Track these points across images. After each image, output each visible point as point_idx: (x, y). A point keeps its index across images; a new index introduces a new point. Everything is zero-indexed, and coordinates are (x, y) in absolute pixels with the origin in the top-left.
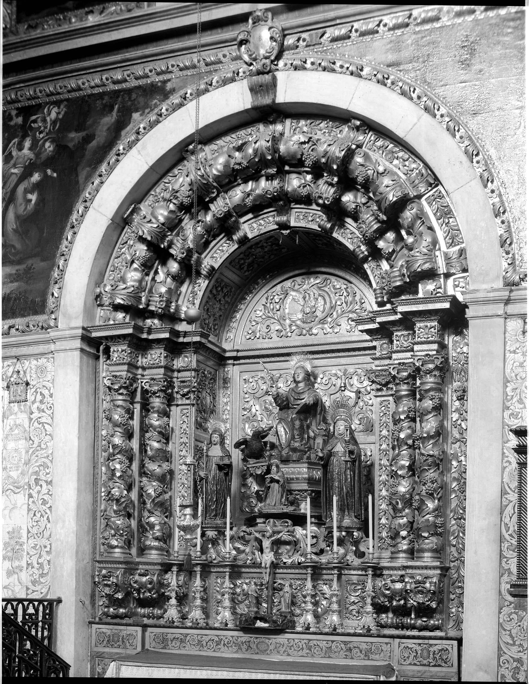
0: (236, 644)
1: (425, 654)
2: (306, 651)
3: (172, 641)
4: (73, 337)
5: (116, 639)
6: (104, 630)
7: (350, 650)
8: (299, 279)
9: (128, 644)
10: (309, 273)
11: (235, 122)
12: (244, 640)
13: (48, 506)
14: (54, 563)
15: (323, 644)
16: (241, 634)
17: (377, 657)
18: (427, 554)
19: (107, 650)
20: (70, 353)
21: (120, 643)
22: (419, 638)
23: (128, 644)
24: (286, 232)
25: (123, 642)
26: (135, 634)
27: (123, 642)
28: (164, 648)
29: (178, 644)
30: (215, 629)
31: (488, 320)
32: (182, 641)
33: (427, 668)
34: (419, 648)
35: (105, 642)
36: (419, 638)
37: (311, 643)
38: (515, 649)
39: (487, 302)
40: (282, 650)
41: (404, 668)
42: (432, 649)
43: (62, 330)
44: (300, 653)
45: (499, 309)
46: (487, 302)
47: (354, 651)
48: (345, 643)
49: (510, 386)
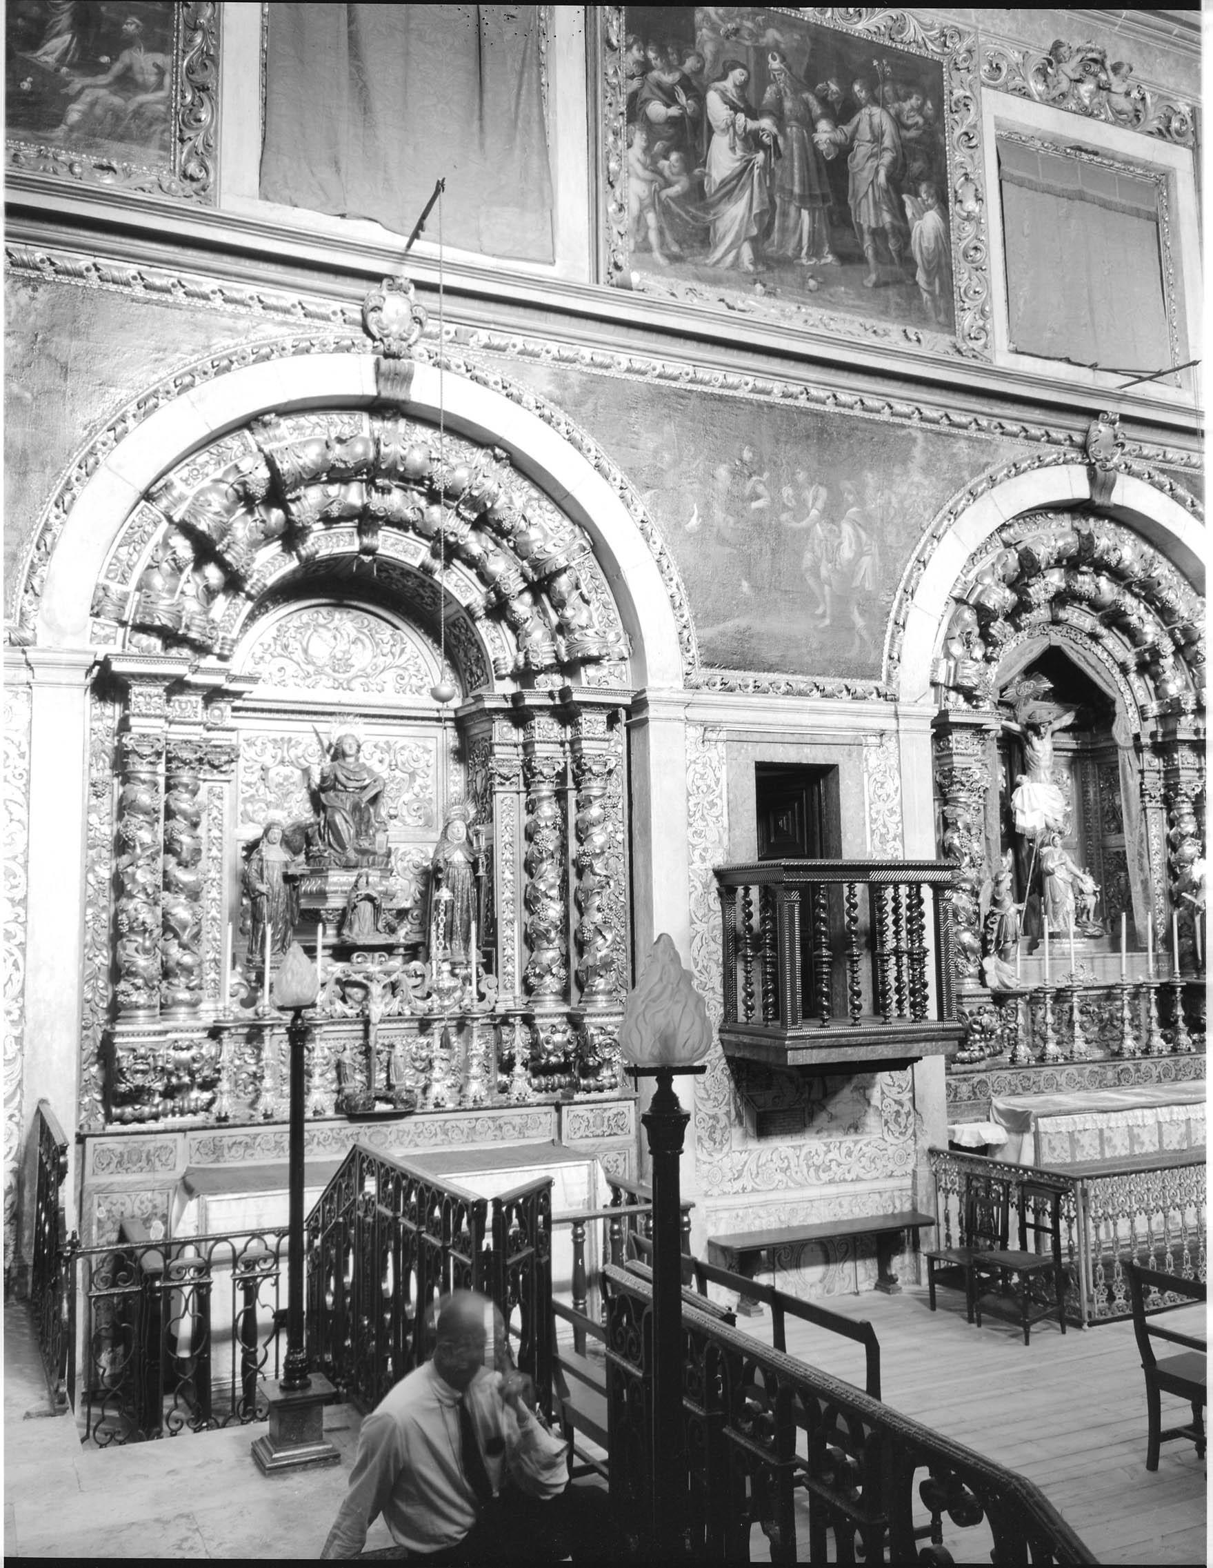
0: (336, 1140)
1: (598, 1122)
2: (441, 1137)
3: (230, 1148)
4: (74, 665)
5: (135, 1158)
6: (111, 1146)
7: (500, 1127)
8: (324, 610)
9: (158, 1164)
10: (339, 605)
11: (353, 402)
12: (349, 1132)
13: (17, 941)
14: (31, 1042)
15: (517, 1121)
16: (346, 1124)
17: (534, 1132)
18: (600, 997)
19: (117, 1178)
20: (64, 690)
21: (143, 1164)
22: (588, 1102)
23: (158, 1164)
24: (367, 559)
25: (149, 1161)
26: (171, 1145)
27: (149, 1161)
28: (217, 1160)
29: (241, 1151)
30: (486, 1109)
31: (669, 724)
32: (247, 1146)
33: (600, 1140)
34: (590, 1115)
35: (113, 1166)
36: (588, 1102)
37: (448, 1125)
38: (710, 1103)
39: (668, 703)
40: (406, 1139)
41: (574, 1143)
42: (606, 1115)
43: (43, 651)
44: (433, 1141)
45: (681, 712)
46: (668, 703)
47: (505, 1128)
48: (493, 1119)
49: (693, 800)
